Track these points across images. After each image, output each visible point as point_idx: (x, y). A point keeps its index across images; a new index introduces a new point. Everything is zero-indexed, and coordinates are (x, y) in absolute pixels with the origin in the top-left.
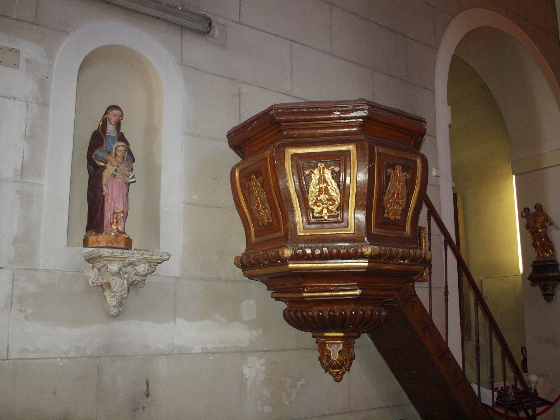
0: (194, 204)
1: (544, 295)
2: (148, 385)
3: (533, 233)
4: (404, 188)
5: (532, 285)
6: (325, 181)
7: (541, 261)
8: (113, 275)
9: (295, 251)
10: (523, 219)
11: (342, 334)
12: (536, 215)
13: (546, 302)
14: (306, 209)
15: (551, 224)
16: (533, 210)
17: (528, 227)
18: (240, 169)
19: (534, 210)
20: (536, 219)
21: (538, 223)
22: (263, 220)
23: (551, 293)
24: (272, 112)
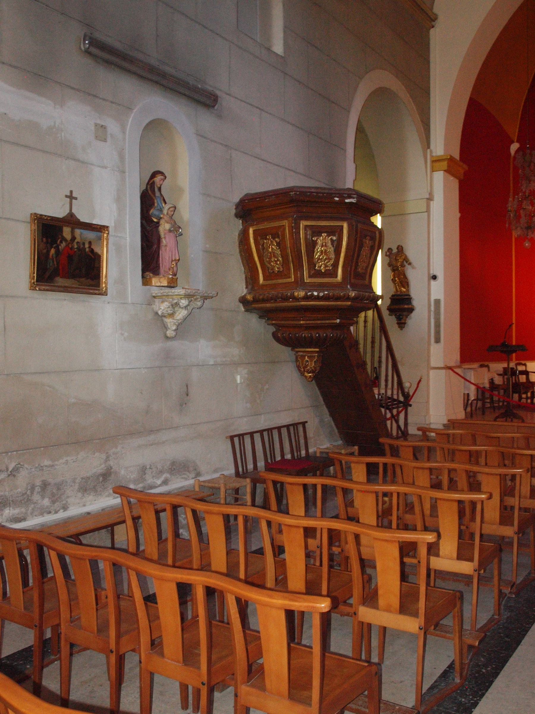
1: (398, 323)
6: (326, 246)
7: (399, 295)
8: (182, 308)
11: (317, 350)
13: (399, 329)
14: (312, 264)
15: (410, 264)
17: (390, 265)
18: (255, 229)
24: (291, 193)
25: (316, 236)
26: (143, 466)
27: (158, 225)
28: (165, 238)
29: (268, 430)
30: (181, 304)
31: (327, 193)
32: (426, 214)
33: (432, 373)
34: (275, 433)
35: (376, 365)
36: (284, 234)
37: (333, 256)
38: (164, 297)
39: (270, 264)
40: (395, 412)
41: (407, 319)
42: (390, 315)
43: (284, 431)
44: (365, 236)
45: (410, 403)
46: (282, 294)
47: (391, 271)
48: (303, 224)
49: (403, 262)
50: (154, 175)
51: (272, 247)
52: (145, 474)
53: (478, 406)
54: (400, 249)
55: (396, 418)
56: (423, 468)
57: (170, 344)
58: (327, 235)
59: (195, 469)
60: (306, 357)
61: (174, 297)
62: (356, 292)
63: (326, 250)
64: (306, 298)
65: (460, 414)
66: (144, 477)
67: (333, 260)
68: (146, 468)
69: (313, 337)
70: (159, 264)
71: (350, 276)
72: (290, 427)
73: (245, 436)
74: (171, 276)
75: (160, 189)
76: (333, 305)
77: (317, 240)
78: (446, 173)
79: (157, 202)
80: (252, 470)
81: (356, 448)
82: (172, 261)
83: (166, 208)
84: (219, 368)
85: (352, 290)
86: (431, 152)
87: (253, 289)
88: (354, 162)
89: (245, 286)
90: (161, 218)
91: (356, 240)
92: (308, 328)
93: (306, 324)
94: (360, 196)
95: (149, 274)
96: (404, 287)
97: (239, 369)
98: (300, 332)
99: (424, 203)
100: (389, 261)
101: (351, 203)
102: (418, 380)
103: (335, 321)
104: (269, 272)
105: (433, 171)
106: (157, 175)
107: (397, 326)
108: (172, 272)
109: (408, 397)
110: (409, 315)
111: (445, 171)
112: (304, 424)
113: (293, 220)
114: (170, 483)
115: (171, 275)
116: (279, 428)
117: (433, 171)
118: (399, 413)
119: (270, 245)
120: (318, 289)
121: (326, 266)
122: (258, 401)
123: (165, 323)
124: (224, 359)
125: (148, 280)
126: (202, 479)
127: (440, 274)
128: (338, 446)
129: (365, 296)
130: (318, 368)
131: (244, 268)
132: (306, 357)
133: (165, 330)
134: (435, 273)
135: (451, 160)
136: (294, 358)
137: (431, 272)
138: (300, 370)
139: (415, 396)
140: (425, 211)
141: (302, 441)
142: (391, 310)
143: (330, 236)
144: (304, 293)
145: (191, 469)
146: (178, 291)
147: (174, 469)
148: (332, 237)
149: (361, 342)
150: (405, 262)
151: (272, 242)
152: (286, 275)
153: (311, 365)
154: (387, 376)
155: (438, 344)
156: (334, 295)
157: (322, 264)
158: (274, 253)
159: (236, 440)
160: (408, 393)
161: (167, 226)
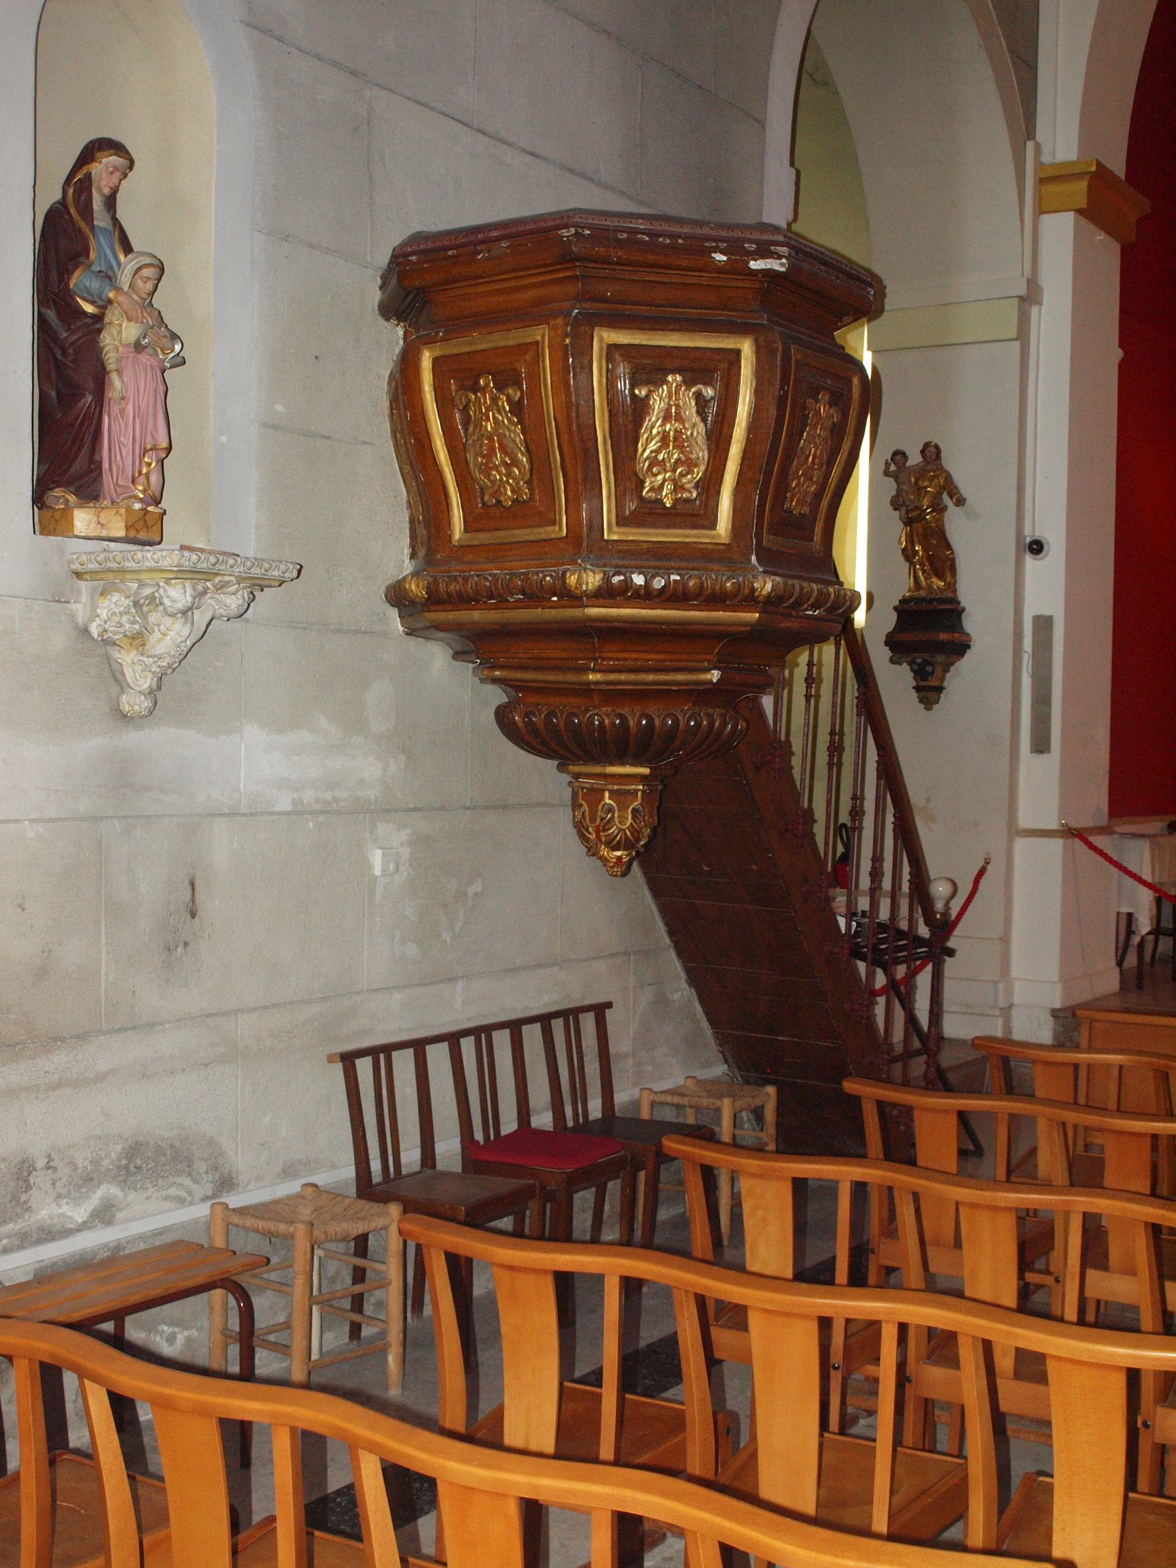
0: (275, 427)
1: (918, 689)
2: (193, 889)
3: (908, 522)
4: (827, 443)
5: (892, 661)
6: (679, 418)
7: (923, 599)
8: (173, 615)
9: (607, 580)
10: (888, 479)
11: (646, 771)
12: (921, 473)
15: (960, 502)
16: (914, 459)
17: (896, 504)
18: (439, 353)
19: (919, 459)
20: (920, 483)
21: (925, 495)
22: (498, 491)
23: (936, 683)
25: (646, 383)
26: (23, 1162)
27: (98, 326)
28: (119, 372)
29: (475, 1032)
30: (167, 602)
31: (686, 237)
32: (1017, 344)
33: (1020, 844)
34: (502, 1041)
35: (844, 818)
36: (535, 377)
37: (701, 453)
38: (110, 576)
39: (488, 476)
40: (901, 971)
41: (948, 675)
42: (892, 661)
43: (532, 1035)
44: (814, 393)
45: (951, 944)
46: (526, 578)
47: (901, 525)
48: (601, 339)
49: (938, 496)
50: (90, 153)
51: (494, 417)
52: (29, 1188)
53: (1160, 949)
54: (932, 453)
55: (901, 992)
56: (994, 1209)
57: (131, 738)
58: (685, 382)
59: (216, 1168)
60: (607, 794)
61: (143, 576)
62: (778, 579)
63: (678, 433)
64: (606, 594)
65: (1110, 981)
66: (24, 1197)
67: (703, 468)
68: (32, 1169)
69: (628, 727)
70: (101, 463)
71: (760, 526)
72: (553, 1022)
73: (395, 1055)
74: (137, 506)
75: (111, 202)
76: (699, 623)
77: (648, 396)
78: (1084, 221)
79: (101, 248)
80: (417, 1167)
81: (771, 1090)
82: (146, 451)
83: (128, 265)
84: (311, 825)
85: (765, 572)
86: (1038, 147)
87: (430, 561)
88: (792, 164)
89: (407, 551)
90: (110, 302)
91: (781, 402)
92: (613, 695)
93: (608, 683)
94: (801, 250)
95: (59, 496)
96: (940, 577)
97: (382, 828)
98: (587, 710)
99: (1011, 311)
100: (894, 493)
101: (768, 273)
102: (976, 871)
103: (708, 676)
104: (484, 503)
105: (1041, 209)
106: (98, 154)
107: (914, 695)
108: (144, 492)
109: (944, 927)
110: (953, 664)
111: (1080, 212)
112: (600, 1010)
113: (567, 325)
114: (120, 1216)
115: (141, 500)
116: (515, 1027)
117: (1042, 213)
118: (912, 973)
119: (488, 410)
120: (647, 563)
121: (678, 487)
122: (446, 936)
123: (115, 666)
124: (328, 796)
125: (57, 515)
126: (235, 1201)
127: (1055, 537)
128: (715, 1082)
129: (810, 594)
130: (647, 831)
131: (408, 492)
132: (607, 794)
133: (114, 689)
134: (1038, 534)
135: (1100, 176)
136: (567, 793)
137: (1027, 531)
138: (583, 838)
139: (965, 917)
140: (1015, 336)
141: (592, 1068)
142: (897, 645)
143: (694, 384)
144: (599, 577)
145: (201, 1167)
146: (165, 556)
147: (138, 1168)
148: (701, 386)
149: (797, 745)
150: (945, 497)
151: (495, 400)
152: (540, 513)
153: (623, 823)
154: (877, 859)
155: (1044, 757)
156: (701, 587)
157: (664, 480)
158: (501, 437)
159: (364, 1067)
160: (946, 914)
161: (131, 331)
